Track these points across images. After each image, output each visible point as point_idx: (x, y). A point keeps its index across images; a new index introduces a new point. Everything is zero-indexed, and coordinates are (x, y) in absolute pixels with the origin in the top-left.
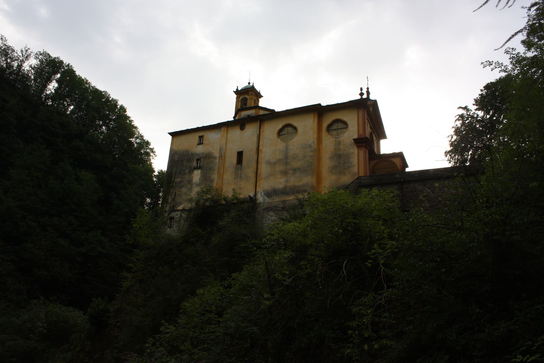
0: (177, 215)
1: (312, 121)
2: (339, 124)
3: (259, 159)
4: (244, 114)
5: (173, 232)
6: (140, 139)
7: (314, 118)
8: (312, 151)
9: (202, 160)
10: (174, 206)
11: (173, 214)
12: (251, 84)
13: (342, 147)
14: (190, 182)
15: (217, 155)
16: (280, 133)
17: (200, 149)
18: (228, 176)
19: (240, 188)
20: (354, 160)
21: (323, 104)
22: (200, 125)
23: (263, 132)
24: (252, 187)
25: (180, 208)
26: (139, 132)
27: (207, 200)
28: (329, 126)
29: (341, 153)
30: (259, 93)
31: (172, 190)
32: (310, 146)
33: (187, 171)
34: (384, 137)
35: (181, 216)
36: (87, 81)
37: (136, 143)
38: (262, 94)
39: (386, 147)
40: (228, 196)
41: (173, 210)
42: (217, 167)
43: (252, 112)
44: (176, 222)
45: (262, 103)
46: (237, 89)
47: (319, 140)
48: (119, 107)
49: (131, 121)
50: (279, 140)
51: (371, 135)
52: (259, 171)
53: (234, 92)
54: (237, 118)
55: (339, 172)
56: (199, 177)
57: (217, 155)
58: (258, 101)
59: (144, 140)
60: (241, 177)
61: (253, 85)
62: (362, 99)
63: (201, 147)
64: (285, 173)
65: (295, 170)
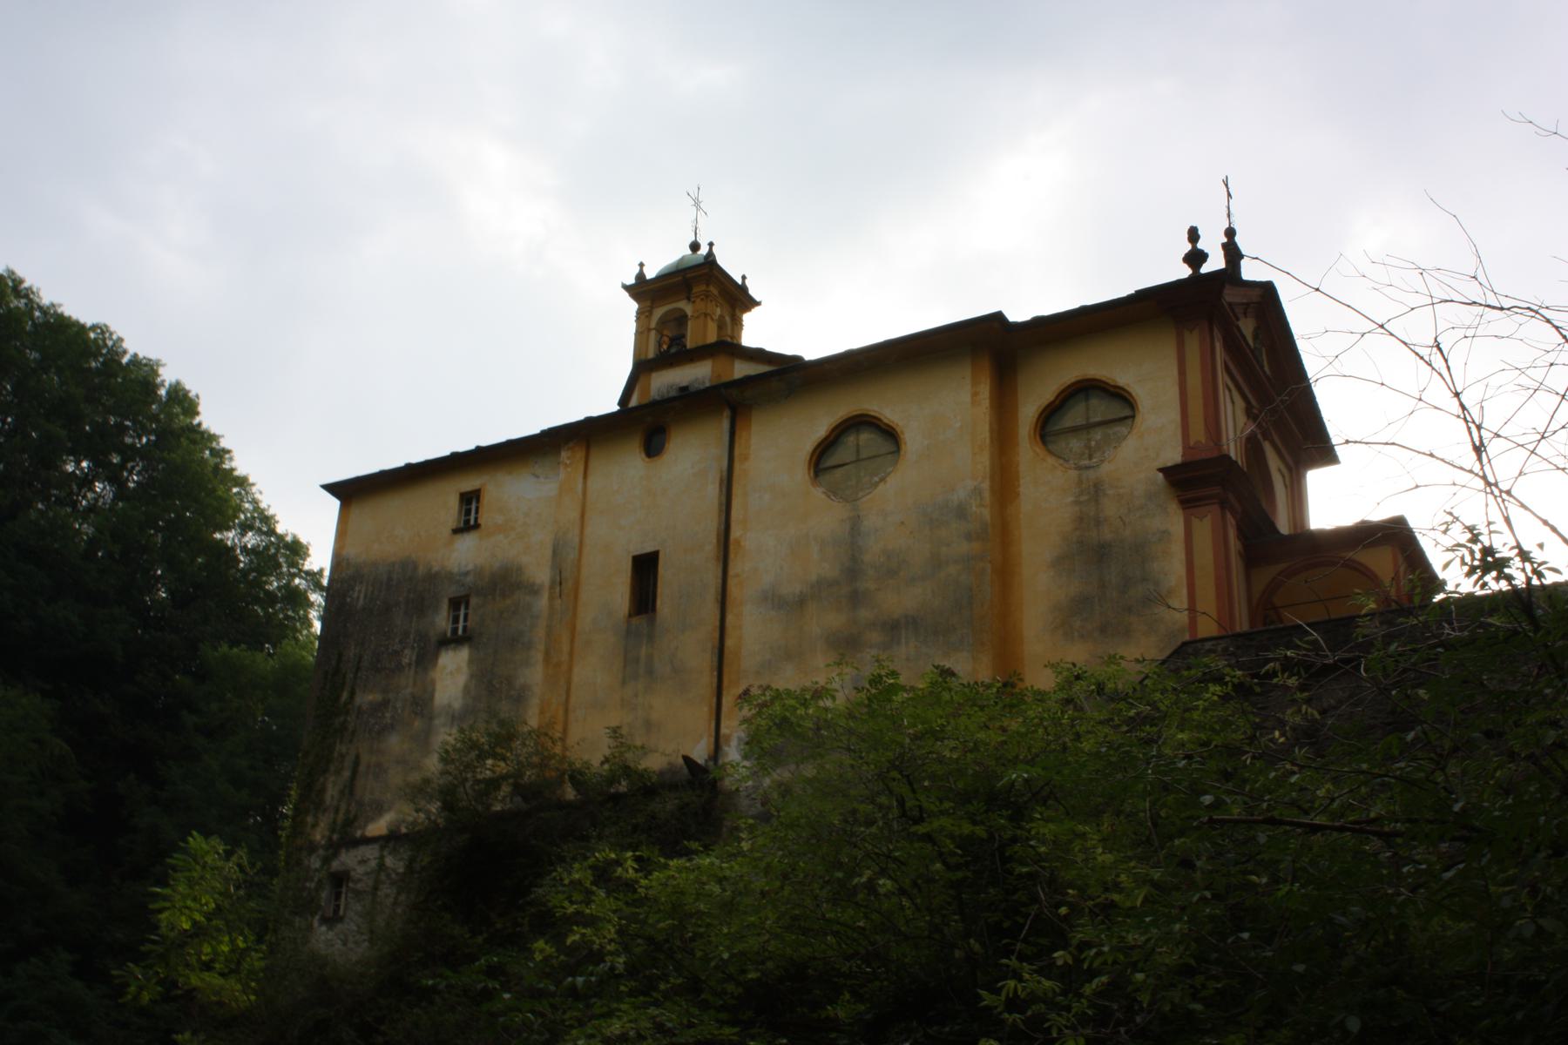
0: (363, 862)
1: (965, 396)
3: (731, 582)
4: (666, 381)
5: (340, 943)
6: (259, 532)
8: (969, 537)
9: (474, 601)
10: (349, 822)
11: (347, 859)
12: (704, 251)
13: (1110, 509)
14: (422, 704)
15: (541, 574)
16: (821, 459)
17: (466, 554)
18: (594, 672)
19: (648, 725)
20: (1172, 569)
21: (1018, 314)
22: (465, 445)
23: (746, 458)
24: (699, 716)
25: (378, 827)
26: (255, 502)
27: (494, 783)
29: (1107, 534)
30: (743, 289)
31: (340, 748)
32: (961, 512)
33: (408, 656)
34: (1323, 452)
35: (381, 866)
36: (18, 282)
37: (244, 549)
38: (753, 292)
39: (1332, 501)
40: (587, 765)
41: (347, 839)
42: (540, 632)
43: (698, 374)
44: (358, 894)
45: (756, 332)
46: (640, 277)
47: (1004, 483)
48: (163, 392)
49: (222, 454)
50: (818, 493)
51: (1253, 446)
52: (729, 643)
53: (627, 288)
54: (633, 402)
55: (1103, 630)
56: (462, 679)
57: (541, 574)
58: (737, 324)
59: (281, 538)
60: (650, 672)
61: (710, 254)
62: (1196, 279)
63: (468, 542)
65: (894, 628)
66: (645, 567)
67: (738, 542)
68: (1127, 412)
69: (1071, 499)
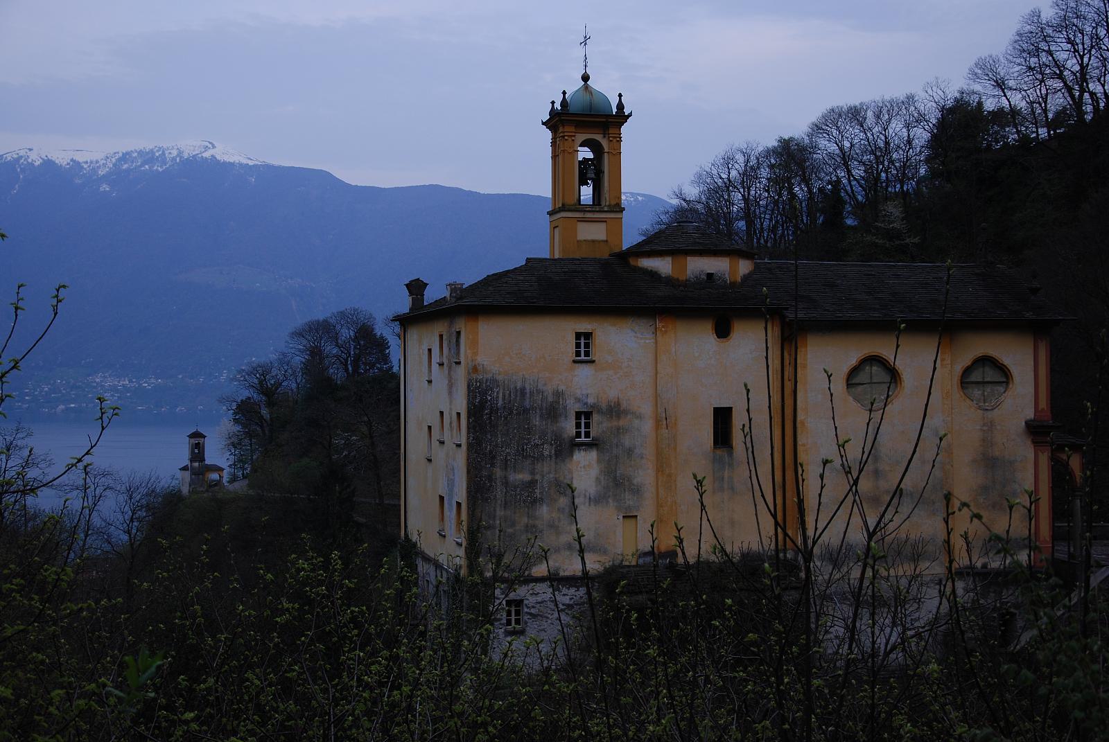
2: (987, 369)
3: (800, 449)
9: (596, 417)
28: (967, 371)
56: (594, 471)
63: (584, 371)
67: (803, 423)
68: (1005, 380)
69: (978, 427)
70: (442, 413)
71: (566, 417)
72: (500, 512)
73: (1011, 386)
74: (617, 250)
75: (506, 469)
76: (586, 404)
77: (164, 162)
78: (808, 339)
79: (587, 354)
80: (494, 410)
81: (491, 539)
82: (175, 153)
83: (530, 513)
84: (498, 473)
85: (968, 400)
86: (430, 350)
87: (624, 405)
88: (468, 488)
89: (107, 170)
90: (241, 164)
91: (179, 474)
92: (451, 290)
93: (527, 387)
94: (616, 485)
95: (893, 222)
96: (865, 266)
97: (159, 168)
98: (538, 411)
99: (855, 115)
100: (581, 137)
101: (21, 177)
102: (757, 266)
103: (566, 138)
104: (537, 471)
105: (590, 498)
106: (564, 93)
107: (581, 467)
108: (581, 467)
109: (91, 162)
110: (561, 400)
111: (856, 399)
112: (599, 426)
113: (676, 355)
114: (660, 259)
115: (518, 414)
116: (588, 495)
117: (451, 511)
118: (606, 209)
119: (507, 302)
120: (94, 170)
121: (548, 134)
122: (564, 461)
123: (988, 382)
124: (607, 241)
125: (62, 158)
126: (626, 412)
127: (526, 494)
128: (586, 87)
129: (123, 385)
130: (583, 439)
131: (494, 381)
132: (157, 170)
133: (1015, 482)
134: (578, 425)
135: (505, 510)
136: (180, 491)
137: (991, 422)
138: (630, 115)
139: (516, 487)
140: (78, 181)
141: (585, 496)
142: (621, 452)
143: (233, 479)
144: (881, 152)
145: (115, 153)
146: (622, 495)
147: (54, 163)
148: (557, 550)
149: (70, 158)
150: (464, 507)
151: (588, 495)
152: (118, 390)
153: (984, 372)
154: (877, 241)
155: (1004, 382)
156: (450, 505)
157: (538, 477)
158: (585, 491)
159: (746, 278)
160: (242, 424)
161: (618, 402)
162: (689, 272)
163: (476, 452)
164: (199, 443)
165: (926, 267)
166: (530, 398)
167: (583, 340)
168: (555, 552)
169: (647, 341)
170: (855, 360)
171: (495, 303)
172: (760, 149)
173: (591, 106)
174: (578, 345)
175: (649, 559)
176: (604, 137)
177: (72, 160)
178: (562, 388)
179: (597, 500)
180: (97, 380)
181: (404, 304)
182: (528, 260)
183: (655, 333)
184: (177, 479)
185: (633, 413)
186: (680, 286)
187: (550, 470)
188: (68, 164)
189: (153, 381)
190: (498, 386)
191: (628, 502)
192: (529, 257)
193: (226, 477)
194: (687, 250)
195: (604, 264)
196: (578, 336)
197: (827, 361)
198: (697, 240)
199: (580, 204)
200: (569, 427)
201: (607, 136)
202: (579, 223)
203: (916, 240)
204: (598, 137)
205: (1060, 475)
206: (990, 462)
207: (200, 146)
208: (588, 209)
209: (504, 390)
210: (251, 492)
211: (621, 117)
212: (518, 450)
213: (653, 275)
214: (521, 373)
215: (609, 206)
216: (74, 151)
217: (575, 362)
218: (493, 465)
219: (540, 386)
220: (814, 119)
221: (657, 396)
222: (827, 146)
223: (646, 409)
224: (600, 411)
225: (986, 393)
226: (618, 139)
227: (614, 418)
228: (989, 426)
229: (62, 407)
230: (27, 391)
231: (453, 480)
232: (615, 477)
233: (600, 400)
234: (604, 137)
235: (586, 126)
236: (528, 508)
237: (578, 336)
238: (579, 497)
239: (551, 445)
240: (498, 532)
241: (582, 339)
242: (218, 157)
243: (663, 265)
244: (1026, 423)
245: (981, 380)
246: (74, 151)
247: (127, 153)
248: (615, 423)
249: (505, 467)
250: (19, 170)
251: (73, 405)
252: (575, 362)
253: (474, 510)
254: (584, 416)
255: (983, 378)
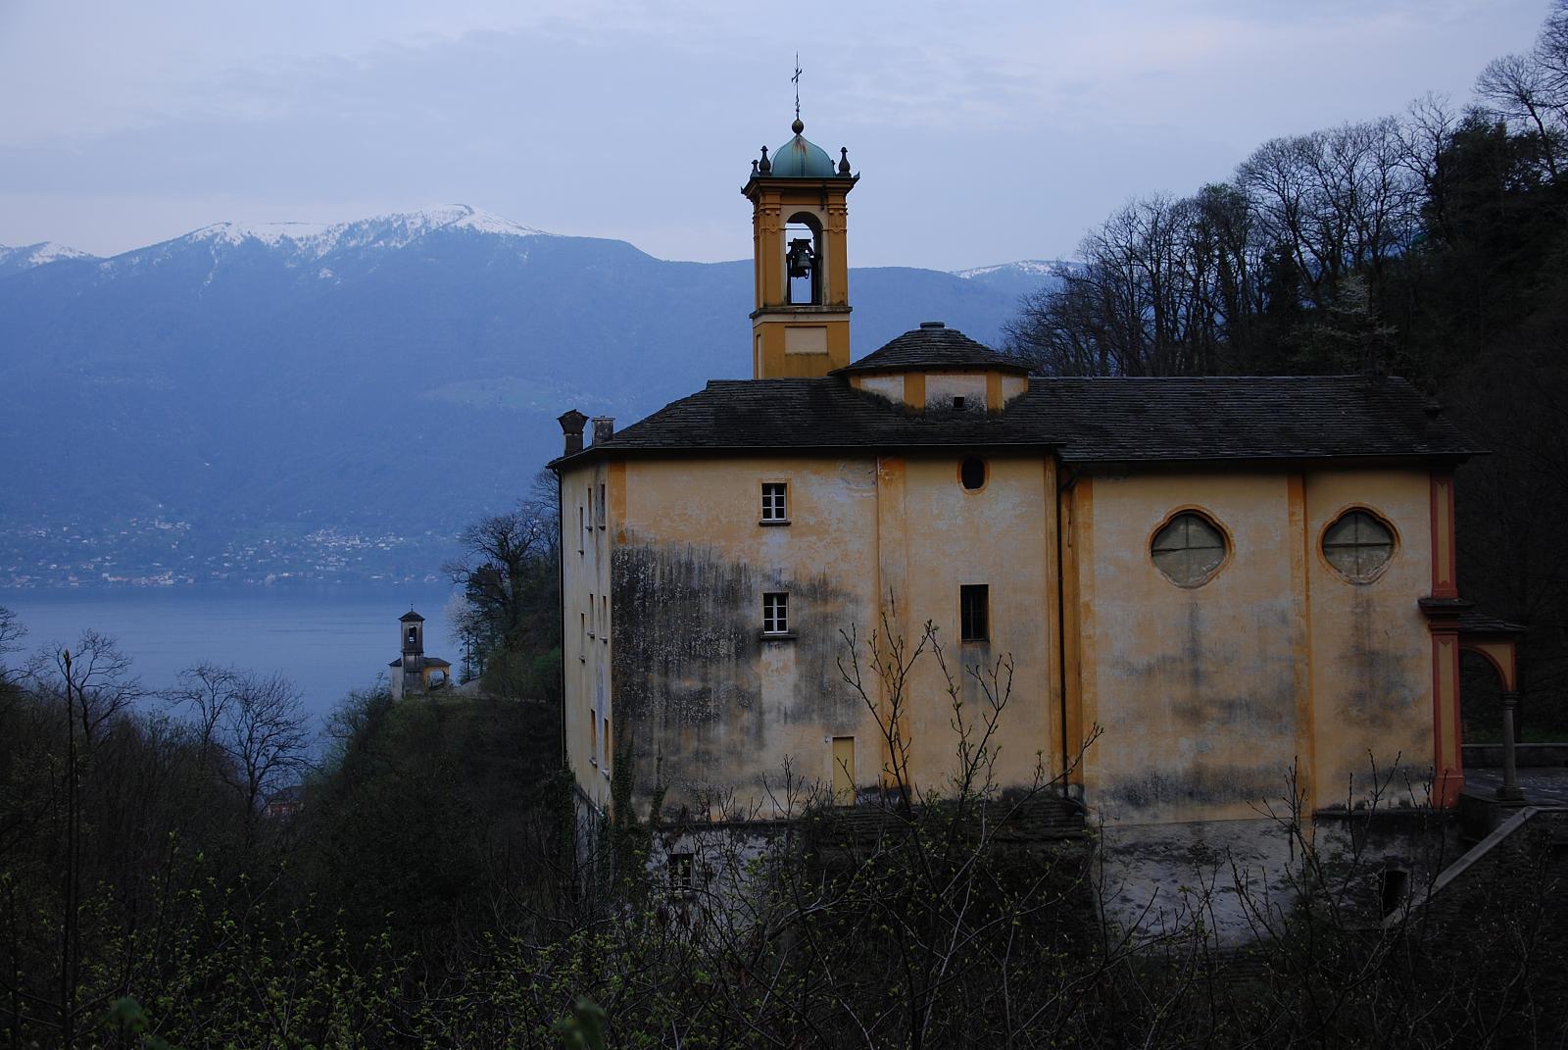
2: (1361, 526)
7: (1291, 504)
9: (792, 602)
14: (747, 699)
16: (1158, 542)
28: (1331, 530)
55: (1373, 720)
56: (792, 676)
63: (775, 538)
64: (1192, 715)
66: (974, 599)
67: (1087, 606)
68: (1387, 541)
69: (1349, 609)
70: (592, 595)
71: (750, 601)
72: (659, 734)
73: (1396, 550)
74: (841, 366)
75: (666, 674)
76: (779, 583)
77: (405, 236)
78: (1094, 484)
79: (780, 513)
80: (649, 593)
81: (646, 771)
82: (419, 222)
83: (702, 734)
84: (656, 679)
85: (1332, 571)
86: (581, 509)
87: (833, 584)
88: (613, 701)
89: (329, 248)
90: (508, 236)
91: (390, 672)
92: (597, 428)
93: (696, 562)
94: (822, 695)
95: (1357, 305)
96: (1193, 381)
97: (398, 244)
98: (710, 593)
99: (1306, 150)
100: (791, 210)
101: (217, 262)
102: (1033, 387)
103: (768, 212)
104: (709, 676)
105: (786, 713)
106: (764, 150)
107: (772, 671)
108: (772, 671)
109: (308, 239)
110: (743, 578)
111: (1166, 572)
112: (797, 613)
113: (906, 514)
114: (888, 378)
115: (683, 598)
116: (782, 708)
117: (600, 732)
118: (825, 309)
119: (664, 444)
120: (312, 250)
121: (749, 207)
122: (748, 662)
123: (1362, 545)
124: (827, 354)
125: (268, 235)
126: (836, 593)
127: (695, 708)
128: (798, 141)
129: (353, 546)
130: (776, 631)
131: (648, 552)
132: (395, 247)
133: (1404, 686)
134: (768, 613)
135: (665, 730)
136: (390, 695)
137: (1368, 601)
138: (856, 179)
139: (681, 699)
140: (290, 265)
141: (779, 709)
142: (829, 649)
143: (467, 678)
144: (1349, 202)
145: (339, 226)
146: (832, 709)
147: (258, 240)
148: (741, 786)
149: (280, 233)
150: (610, 723)
151: (782, 708)
152: (345, 552)
153: (1356, 530)
154: (1333, 333)
155: (1386, 544)
156: (600, 722)
157: (711, 685)
158: (780, 703)
159: (1012, 404)
160: (480, 601)
161: (824, 579)
162: (928, 397)
163: (624, 651)
164: (415, 628)
165: (1286, 381)
166: (700, 577)
167: (774, 493)
168: (737, 789)
169: (865, 495)
170: (1163, 516)
171: (647, 445)
172: (1173, 202)
173: (803, 168)
174: (767, 502)
175: (874, 798)
176: (823, 209)
177: (282, 237)
178: (743, 561)
179: (795, 717)
180: (318, 539)
181: (557, 449)
182: (710, 384)
183: (875, 483)
184: (386, 678)
185: (846, 595)
186: (916, 416)
187: (729, 675)
188: (278, 242)
189: (392, 539)
190: (654, 559)
191: (840, 719)
192: (711, 379)
193: (455, 675)
194: (925, 366)
195: (816, 388)
196: (767, 488)
197: (1121, 520)
198: (943, 352)
199: (789, 303)
200: (755, 615)
201: (826, 207)
202: (788, 331)
203: (1393, 330)
204: (814, 210)
205: (1474, 677)
206: (1366, 658)
207: (453, 211)
208: (799, 310)
209: (662, 564)
210: (484, 697)
211: (845, 181)
212: (683, 648)
213: (880, 402)
214: (686, 542)
215: (831, 305)
216: (285, 223)
217: (762, 525)
218: (648, 669)
219: (713, 560)
220: (1245, 160)
221: (879, 570)
222: (1265, 199)
223: (865, 588)
224: (798, 593)
225: (1360, 561)
226: (842, 212)
227: (819, 602)
228: (1365, 608)
229: (271, 577)
230: (226, 555)
231: (601, 688)
232: (821, 685)
233: (798, 577)
234: (823, 209)
235: (800, 190)
236: (698, 727)
237: (767, 488)
238: (770, 712)
239: (730, 639)
240: (655, 761)
241: (773, 492)
242: (478, 227)
243: (892, 388)
244: (1419, 601)
245: (1353, 542)
246: (285, 223)
247: (356, 225)
248: (821, 609)
249: (666, 670)
250: (213, 252)
251: (287, 574)
252: (762, 525)
253: (622, 730)
254: (776, 600)
255: (1357, 539)
